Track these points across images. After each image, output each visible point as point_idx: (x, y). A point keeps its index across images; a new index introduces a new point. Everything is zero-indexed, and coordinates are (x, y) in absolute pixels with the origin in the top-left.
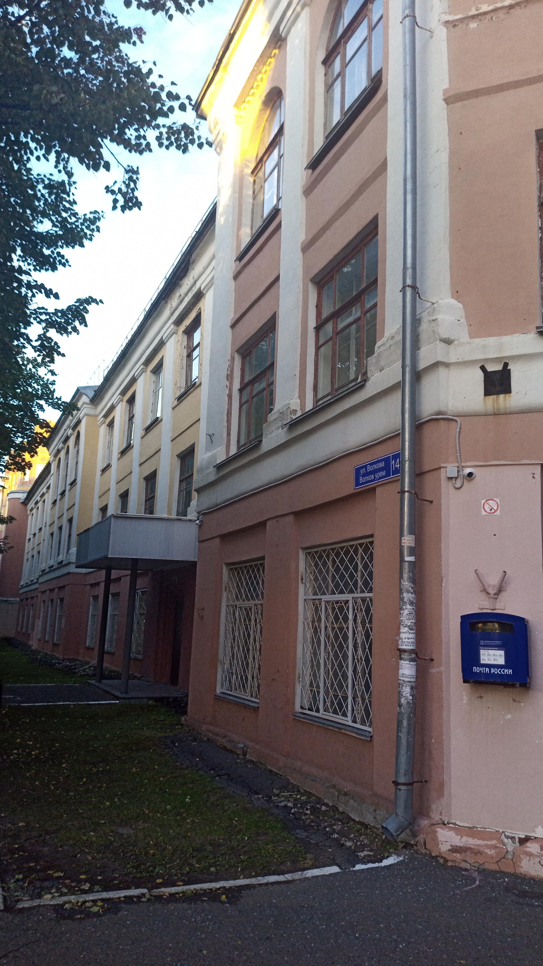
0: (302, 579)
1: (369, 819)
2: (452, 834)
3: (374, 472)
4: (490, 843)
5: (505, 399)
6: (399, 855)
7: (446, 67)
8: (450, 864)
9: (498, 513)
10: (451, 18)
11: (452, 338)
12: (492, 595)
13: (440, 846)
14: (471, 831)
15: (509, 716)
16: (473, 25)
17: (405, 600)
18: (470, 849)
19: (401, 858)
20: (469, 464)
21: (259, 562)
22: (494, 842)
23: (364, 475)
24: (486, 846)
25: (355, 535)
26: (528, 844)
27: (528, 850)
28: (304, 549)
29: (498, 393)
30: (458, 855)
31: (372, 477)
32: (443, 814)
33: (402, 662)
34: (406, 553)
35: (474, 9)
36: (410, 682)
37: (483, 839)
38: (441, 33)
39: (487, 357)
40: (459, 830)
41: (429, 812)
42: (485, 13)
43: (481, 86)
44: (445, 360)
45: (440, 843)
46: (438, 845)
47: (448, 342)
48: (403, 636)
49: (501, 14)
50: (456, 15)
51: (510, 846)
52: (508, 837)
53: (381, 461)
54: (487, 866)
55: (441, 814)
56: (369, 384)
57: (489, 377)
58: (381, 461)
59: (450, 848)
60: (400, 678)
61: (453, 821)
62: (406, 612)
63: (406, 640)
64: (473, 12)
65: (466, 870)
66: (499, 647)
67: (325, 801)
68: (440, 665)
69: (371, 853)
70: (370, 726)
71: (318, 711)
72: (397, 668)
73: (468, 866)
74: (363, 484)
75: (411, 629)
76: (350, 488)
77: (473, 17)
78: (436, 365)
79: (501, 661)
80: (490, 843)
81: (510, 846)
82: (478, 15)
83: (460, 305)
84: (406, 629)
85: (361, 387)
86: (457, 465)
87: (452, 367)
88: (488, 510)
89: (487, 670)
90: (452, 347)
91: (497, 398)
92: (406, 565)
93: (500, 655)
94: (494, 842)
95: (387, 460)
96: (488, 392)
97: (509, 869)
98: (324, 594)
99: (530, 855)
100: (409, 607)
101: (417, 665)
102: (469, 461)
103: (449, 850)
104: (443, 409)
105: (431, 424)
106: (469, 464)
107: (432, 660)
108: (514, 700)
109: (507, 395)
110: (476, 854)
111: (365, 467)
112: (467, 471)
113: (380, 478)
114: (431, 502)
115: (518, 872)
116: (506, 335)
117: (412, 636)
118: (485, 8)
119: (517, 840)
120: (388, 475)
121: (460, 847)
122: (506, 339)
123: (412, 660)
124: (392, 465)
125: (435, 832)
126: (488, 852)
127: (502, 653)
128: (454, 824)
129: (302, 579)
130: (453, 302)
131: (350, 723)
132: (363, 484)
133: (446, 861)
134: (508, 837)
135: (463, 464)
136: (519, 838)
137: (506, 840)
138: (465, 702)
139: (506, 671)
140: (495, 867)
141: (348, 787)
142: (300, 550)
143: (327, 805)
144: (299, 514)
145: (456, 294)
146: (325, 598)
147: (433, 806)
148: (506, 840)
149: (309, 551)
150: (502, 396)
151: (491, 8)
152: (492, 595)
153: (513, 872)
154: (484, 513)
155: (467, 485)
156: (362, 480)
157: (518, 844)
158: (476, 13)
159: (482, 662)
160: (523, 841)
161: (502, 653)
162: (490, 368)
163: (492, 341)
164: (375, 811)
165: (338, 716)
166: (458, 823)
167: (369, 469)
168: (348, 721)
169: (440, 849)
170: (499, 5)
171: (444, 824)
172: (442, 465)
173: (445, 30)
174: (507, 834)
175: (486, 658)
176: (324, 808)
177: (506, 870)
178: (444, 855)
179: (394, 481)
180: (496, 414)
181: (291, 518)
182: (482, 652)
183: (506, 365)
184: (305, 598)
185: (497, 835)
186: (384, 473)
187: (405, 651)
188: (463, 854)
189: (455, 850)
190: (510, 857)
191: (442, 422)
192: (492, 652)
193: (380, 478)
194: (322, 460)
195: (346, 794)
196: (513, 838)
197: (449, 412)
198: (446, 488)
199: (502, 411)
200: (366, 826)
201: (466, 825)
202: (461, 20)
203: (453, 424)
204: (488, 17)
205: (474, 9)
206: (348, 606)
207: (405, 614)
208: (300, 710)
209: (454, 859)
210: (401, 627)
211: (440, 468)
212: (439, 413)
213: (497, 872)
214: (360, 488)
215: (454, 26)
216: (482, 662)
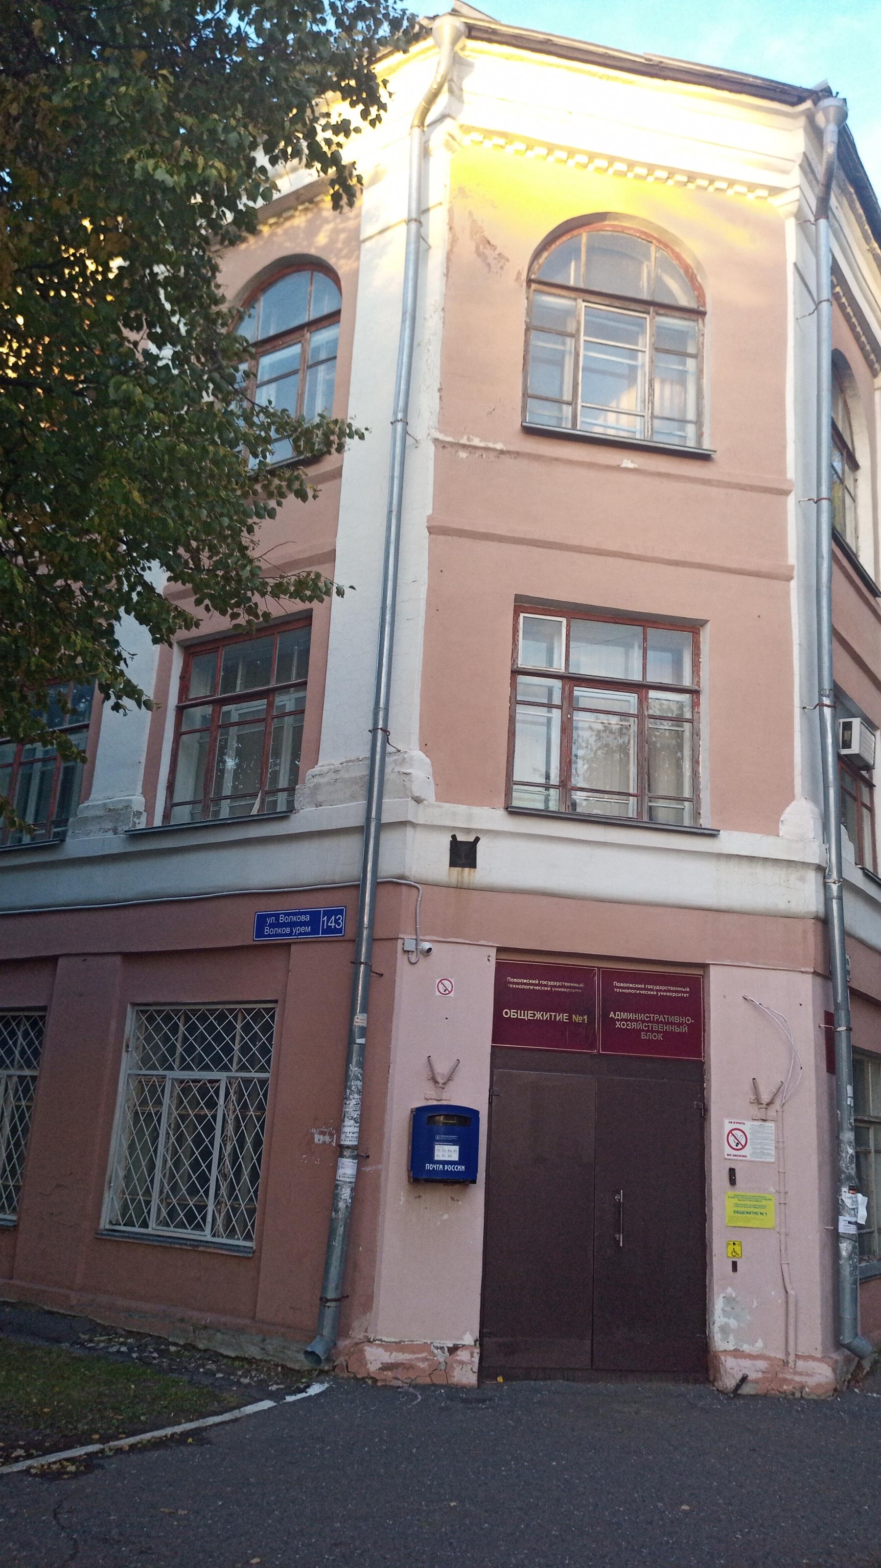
0: (127, 1046)
1: (253, 1351)
2: (381, 1350)
3: (292, 925)
4: (420, 1356)
5: (469, 874)
6: (322, 1383)
7: (430, 489)
8: (379, 1384)
9: (452, 994)
10: (441, 437)
11: (423, 797)
12: (441, 1085)
13: (369, 1366)
14: (399, 1346)
15: (446, 1217)
16: (463, 455)
17: (353, 1088)
18: (402, 1364)
19: (326, 1385)
20: (428, 938)
21: (36, 1014)
22: (424, 1355)
23: (272, 926)
24: (417, 1359)
25: (246, 998)
26: (459, 1352)
27: (458, 1358)
28: (134, 1005)
29: (463, 866)
30: (389, 1373)
31: (288, 930)
32: (369, 1330)
33: (344, 1160)
34: (357, 1034)
35: (465, 437)
36: (351, 1182)
37: (413, 1353)
38: (428, 450)
39: (456, 825)
40: (388, 1346)
41: (349, 1330)
42: (476, 448)
43: (467, 528)
44: (414, 821)
45: (369, 1363)
46: (366, 1364)
47: (418, 800)
48: (347, 1129)
49: (492, 455)
50: (446, 435)
51: (441, 1357)
52: (437, 1348)
53: (305, 913)
54: (420, 1381)
55: (366, 1331)
56: (293, 817)
57: (455, 844)
58: (305, 913)
59: (381, 1366)
60: (338, 1178)
61: (379, 1337)
62: (353, 1102)
63: (351, 1135)
64: (464, 441)
65: (398, 1387)
66: (453, 1142)
67: (170, 1340)
68: (379, 1163)
69: (281, 1386)
70: (248, 1237)
71: (145, 1225)
72: (335, 1168)
73: (400, 1383)
74: (269, 936)
75: (356, 1122)
76: (248, 937)
77: (464, 446)
78: (404, 824)
79: (455, 1157)
80: (420, 1356)
81: (441, 1357)
82: (469, 446)
83: (428, 760)
84: (352, 1122)
85: (283, 817)
86: (414, 937)
87: (418, 829)
88: (442, 991)
89: (441, 1166)
90: (421, 805)
91: (462, 871)
92: (356, 1048)
93: (455, 1151)
94: (424, 1355)
95: (315, 916)
96: (453, 864)
97: (441, 1381)
98: (170, 1068)
99: (462, 1363)
100: (356, 1096)
101: (358, 1163)
102: (430, 935)
103: (380, 1369)
104: (407, 874)
105: (390, 888)
106: (428, 938)
107: (368, 1157)
108: (453, 1199)
109: (472, 870)
110: (408, 1369)
111: (277, 916)
112: (427, 945)
113: (300, 934)
114: (381, 975)
115: (450, 1382)
116: (476, 805)
117: (357, 1130)
118: (476, 442)
119: (446, 1349)
120: (315, 931)
121: (391, 1364)
122: (476, 810)
123: (354, 1157)
124: (323, 922)
125: (362, 1352)
126: (422, 1365)
127: (457, 1148)
128: (381, 1340)
129: (127, 1046)
130: (423, 756)
131: (209, 1238)
132: (269, 936)
133: (375, 1380)
134: (437, 1348)
135: (421, 937)
136: (448, 1348)
137: (435, 1351)
138: (401, 1203)
139: (459, 1167)
140: (428, 1381)
141: (209, 1318)
142: (129, 1008)
143: (175, 1344)
144: (129, 957)
145: (425, 747)
146: (170, 1074)
147: (356, 1324)
148: (435, 1351)
149: (142, 1009)
150: (467, 870)
151: (482, 444)
152: (441, 1085)
153: (445, 1383)
154: (438, 993)
155: (423, 962)
156: (267, 930)
157: (447, 1354)
158: (468, 443)
159: (436, 1158)
160: (453, 1350)
161: (457, 1148)
162: (460, 838)
163: (462, 809)
164: (264, 1340)
165: (184, 1231)
166: (384, 1339)
167: (282, 919)
168: (206, 1235)
169: (368, 1370)
170: (491, 445)
171: (369, 1341)
172: (400, 936)
173: (433, 447)
174: (436, 1345)
175: (441, 1154)
176: (173, 1349)
177: (437, 1382)
178: (372, 1375)
179: (328, 941)
180: (459, 887)
181: (118, 960)
182: (437, 1147)
183: (477, 839)
184: (129, 1072)
185: (425, 1347)
186: (308, 929)
187: (348, 1147)
188: (395, 1371)
189: (386, 1367)
190: (443, 1367)
191: (403, 887)
192: (447, 1147)
193: (300, 934)
194: (194, 892)
195: (205, 1327)
196: (442, 1348)
197: (412, 877)
198: (401, 961)
199: (465, 886)
200: (250, 1361)
201: (393, 1340)
202: (452, 444)
203: (414, 891)
204: (479, 453)
205: (465, 437)
206: (218, 1087)
207: (351, 1105)
208: (108, 1227)
209: (383, 1378)
210: (346, 1119)
211: (397, 939)
212: (402, 877)
213: (430, 1385)
214: (262, 941)
215: (444, 447)
216: (436, 1158)
